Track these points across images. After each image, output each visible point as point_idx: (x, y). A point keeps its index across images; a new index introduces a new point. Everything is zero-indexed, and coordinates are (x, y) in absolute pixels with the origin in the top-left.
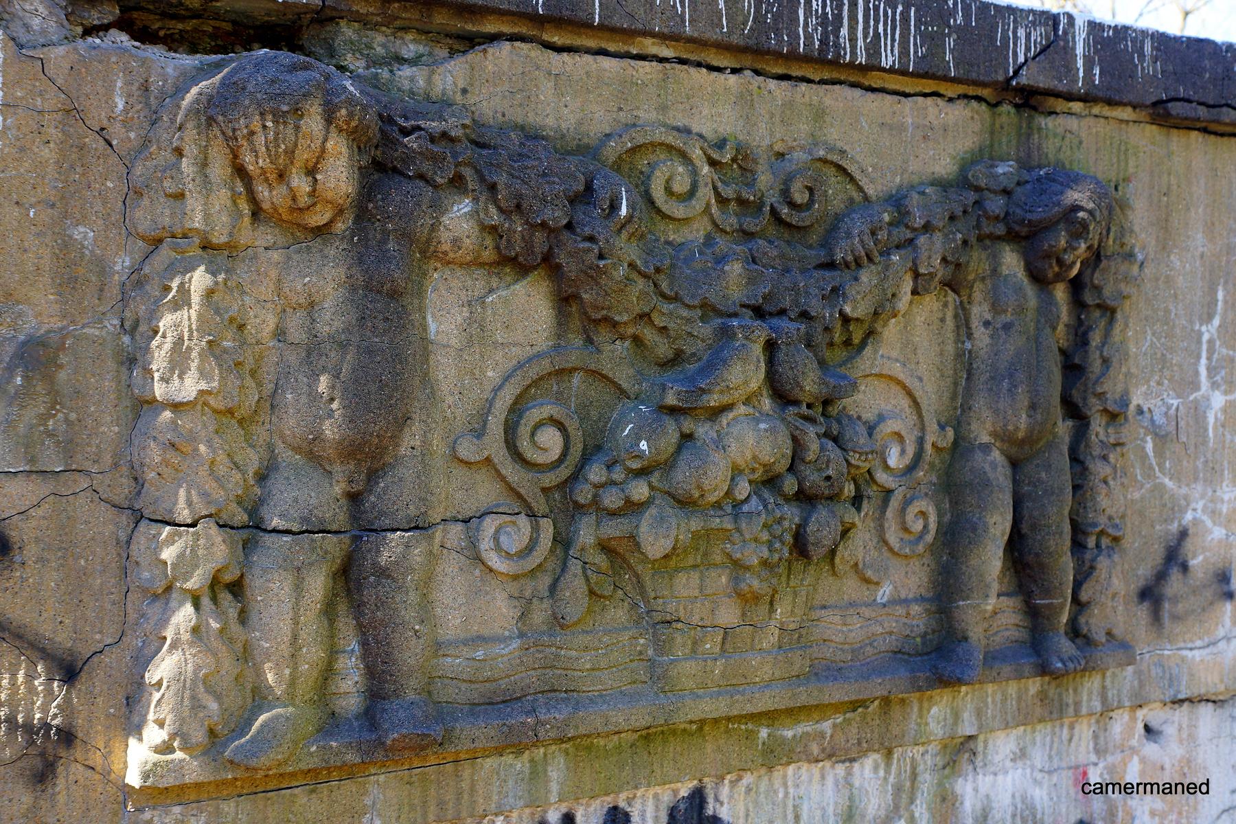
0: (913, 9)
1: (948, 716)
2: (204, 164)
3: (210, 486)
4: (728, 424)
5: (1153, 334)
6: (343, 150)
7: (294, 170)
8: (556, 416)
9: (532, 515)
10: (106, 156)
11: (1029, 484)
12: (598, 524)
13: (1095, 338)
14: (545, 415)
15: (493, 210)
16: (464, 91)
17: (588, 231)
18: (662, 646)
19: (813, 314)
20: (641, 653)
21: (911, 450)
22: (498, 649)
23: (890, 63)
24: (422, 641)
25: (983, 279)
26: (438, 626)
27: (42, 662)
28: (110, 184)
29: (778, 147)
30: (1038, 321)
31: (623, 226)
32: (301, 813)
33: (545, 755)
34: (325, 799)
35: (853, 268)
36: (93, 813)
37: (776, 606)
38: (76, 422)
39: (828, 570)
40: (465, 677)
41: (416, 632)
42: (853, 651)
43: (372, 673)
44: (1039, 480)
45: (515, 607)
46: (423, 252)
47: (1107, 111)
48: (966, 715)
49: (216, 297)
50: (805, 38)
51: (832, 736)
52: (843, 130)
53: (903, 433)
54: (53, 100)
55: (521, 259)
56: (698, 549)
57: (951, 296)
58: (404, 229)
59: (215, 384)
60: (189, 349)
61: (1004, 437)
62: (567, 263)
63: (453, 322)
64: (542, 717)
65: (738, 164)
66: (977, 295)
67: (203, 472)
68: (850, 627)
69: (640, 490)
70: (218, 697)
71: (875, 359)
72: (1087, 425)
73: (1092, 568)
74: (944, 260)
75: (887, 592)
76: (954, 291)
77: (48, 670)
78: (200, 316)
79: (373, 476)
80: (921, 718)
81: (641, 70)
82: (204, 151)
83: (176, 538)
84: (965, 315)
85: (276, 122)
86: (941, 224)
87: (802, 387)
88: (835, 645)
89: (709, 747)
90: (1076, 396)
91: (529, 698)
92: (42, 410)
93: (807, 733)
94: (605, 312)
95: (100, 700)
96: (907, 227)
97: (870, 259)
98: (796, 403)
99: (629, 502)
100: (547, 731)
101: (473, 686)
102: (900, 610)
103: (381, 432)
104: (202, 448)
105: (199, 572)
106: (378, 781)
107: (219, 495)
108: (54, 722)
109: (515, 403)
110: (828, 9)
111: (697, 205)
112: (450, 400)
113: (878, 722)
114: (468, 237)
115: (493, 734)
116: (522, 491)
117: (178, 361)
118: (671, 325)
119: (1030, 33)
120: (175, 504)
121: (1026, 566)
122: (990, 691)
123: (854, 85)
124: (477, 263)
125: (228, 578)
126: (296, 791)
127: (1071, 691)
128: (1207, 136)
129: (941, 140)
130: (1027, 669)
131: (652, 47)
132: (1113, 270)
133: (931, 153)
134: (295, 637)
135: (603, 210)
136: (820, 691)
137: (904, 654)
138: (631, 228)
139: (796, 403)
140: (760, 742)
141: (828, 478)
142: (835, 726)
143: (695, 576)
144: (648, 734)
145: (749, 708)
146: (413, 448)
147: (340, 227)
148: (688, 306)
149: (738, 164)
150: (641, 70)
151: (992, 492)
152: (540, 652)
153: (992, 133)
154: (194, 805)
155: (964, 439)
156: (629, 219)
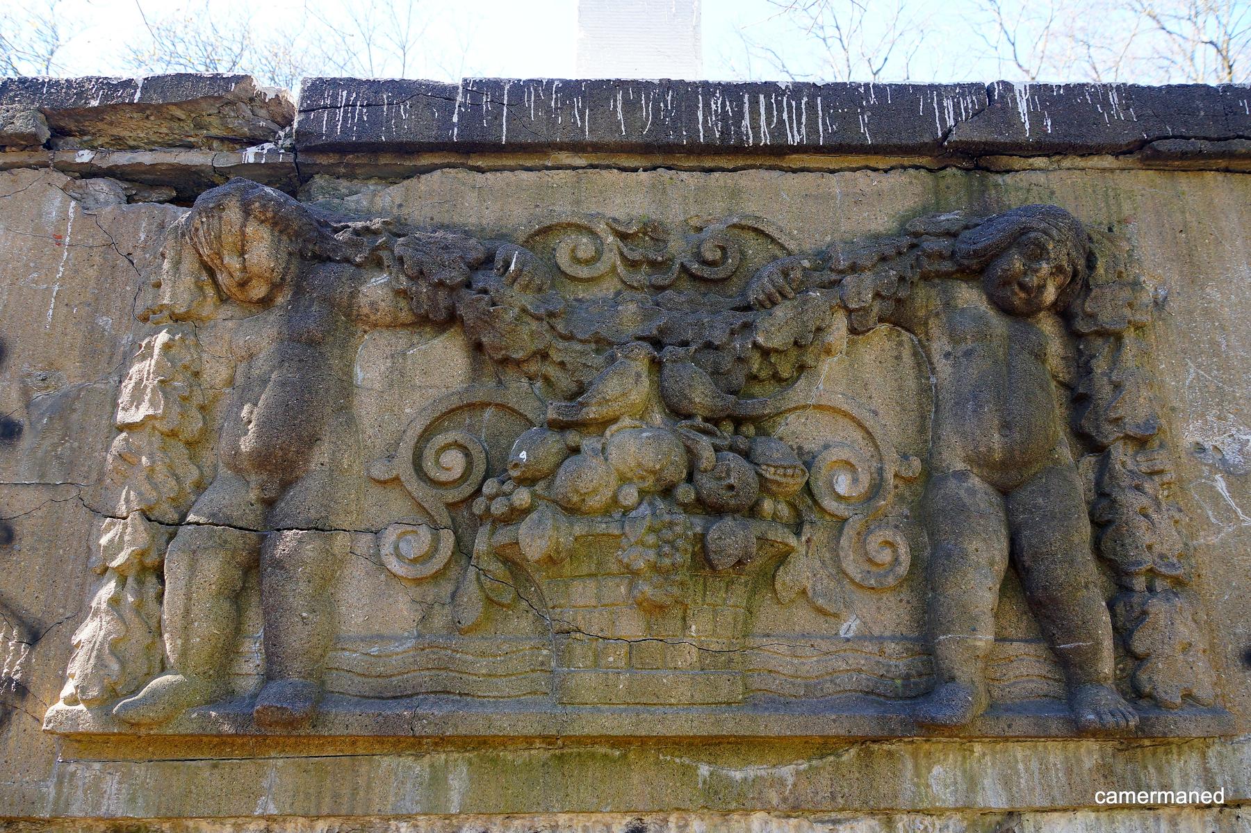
0: (819, 98)
1: (959, 780)
2: (177, 264)
3: (146, 487)
4: (612, 435)
5: (1199, 367)
6: (265, 235)
7: (225, 252)
8: (461, 441)
9: (435, 528)
10: (128, 271)
11: (1023, 513)
12: (493, 533)
13: (1100, 366)
14: (450, 440)
15: (403, 278)
16: (400, 206)
17: (481, 285)
18: (564, 656)
19: (716, 343)
20: (542, 664)
21: (865, 481)
22: (393, 647)
23: (797, 139)
24: (309, 628)
25: (937, 314)
26: (342, 623)
27: (17, 627)
28: (128, 288)
29: (695, 222)
30: (1010, 348)
31: (514, 280)
32: (202, 786)
33: (446, 761)
34: (226, 776)
35: (769, 306)
36: (32, 760)
37: (689, 623)
38: (77, 449)
39: (772, 598)
40: (359, 670)
41: (303, 618)
42: (806, 686)
43: (270, 657)
44: (1035, 506)
45: (416, 610)
46: (348, 315)
47: (1080, 162)
48: (987, 782)
49: (173, 351)
50: (705, 131)
51: (795, 785)
52: (762, 203)
53: (852, 461)
54: (101, 238)
55: (431, 316)
56: (591, 557)
57: (906, 336)
58: (325, 295)
59: (160, 411)
60: (146, 386)
61: (980, 461)
62: (466, 313)
63: (377, 370)
64: (419, 711)
65: (649, 236)
66: (935, 330)
67: (141, 477)
68: (803, 660)
69: (522, 497)
70: (123, 663)
71: (810, 391)
72: (1108, 455)
73: (1145, 613)
74: (877, 295)
75: (853, 627)
76: (908, 330)
77: (20, 634)
78: (157, 363)
79: (286, 486)
80: (918, 777)
81: (556, 177)
82: (179, 253)
83: (112, 527)
84: (925, 352)
85: (207, 217)
86: (869, 264)
87: (690, 399)
88: (783, 678)
89: (636, 778)
90: (1088, 427)
91: (420, 697)
92: (56, 440)
93: (762, 777)
94: (504, 352)
95: (52, 663)
96: (832, 270)
97: (784, 297)
98: (689, 416)
99: (513, 509)
100: (424, 727)
101: (366, 680)
102: (869, 647)
103: (284, 446)
104: (144, 459)
105: (123, 553)
106: (276, 765)
107: (152, 496)
108: (16, 677)
109: (425, 430)
110: (728, 108)
111: (601, 267)
112: (370, 432)
113: (857, 775)
114: (383, 301)
115: (367, 722)
116: (426, 505)
117: (136, 399)
118: (567, 359)
119: (959, 102)
120: (119, 502)
121: (1040, 604)
122: (1019, 756)
123: (771, 168)
124: (394, 325)
125: (151, 560)
126: (200, 763)
127: (1152, 770)
128: (1229, 175)
129: (876, 203)
130: (1054, 727)
131: (565, 158)
132: (1109, 296)
133: (866, 215)
134: (187, 611)
135: (499, 270)
136: (752, 720)
137: (879, 695)
138: (523, 280)
139: (689, 416)
140: (700, 780)
141: (731, 487)
142: (798, 773)
143: (591, 585)
144: (562, 754)
145: (660, 730)
146: (322, 464)
147: (280, 300)
148: (581, 341)
149: (649, 236)
150: (556, 177)
151: (969, 517)
152: (434, 653)
153: (936, 193)
154: (111, 764)
155: (937, 469)
156: (519, 272)
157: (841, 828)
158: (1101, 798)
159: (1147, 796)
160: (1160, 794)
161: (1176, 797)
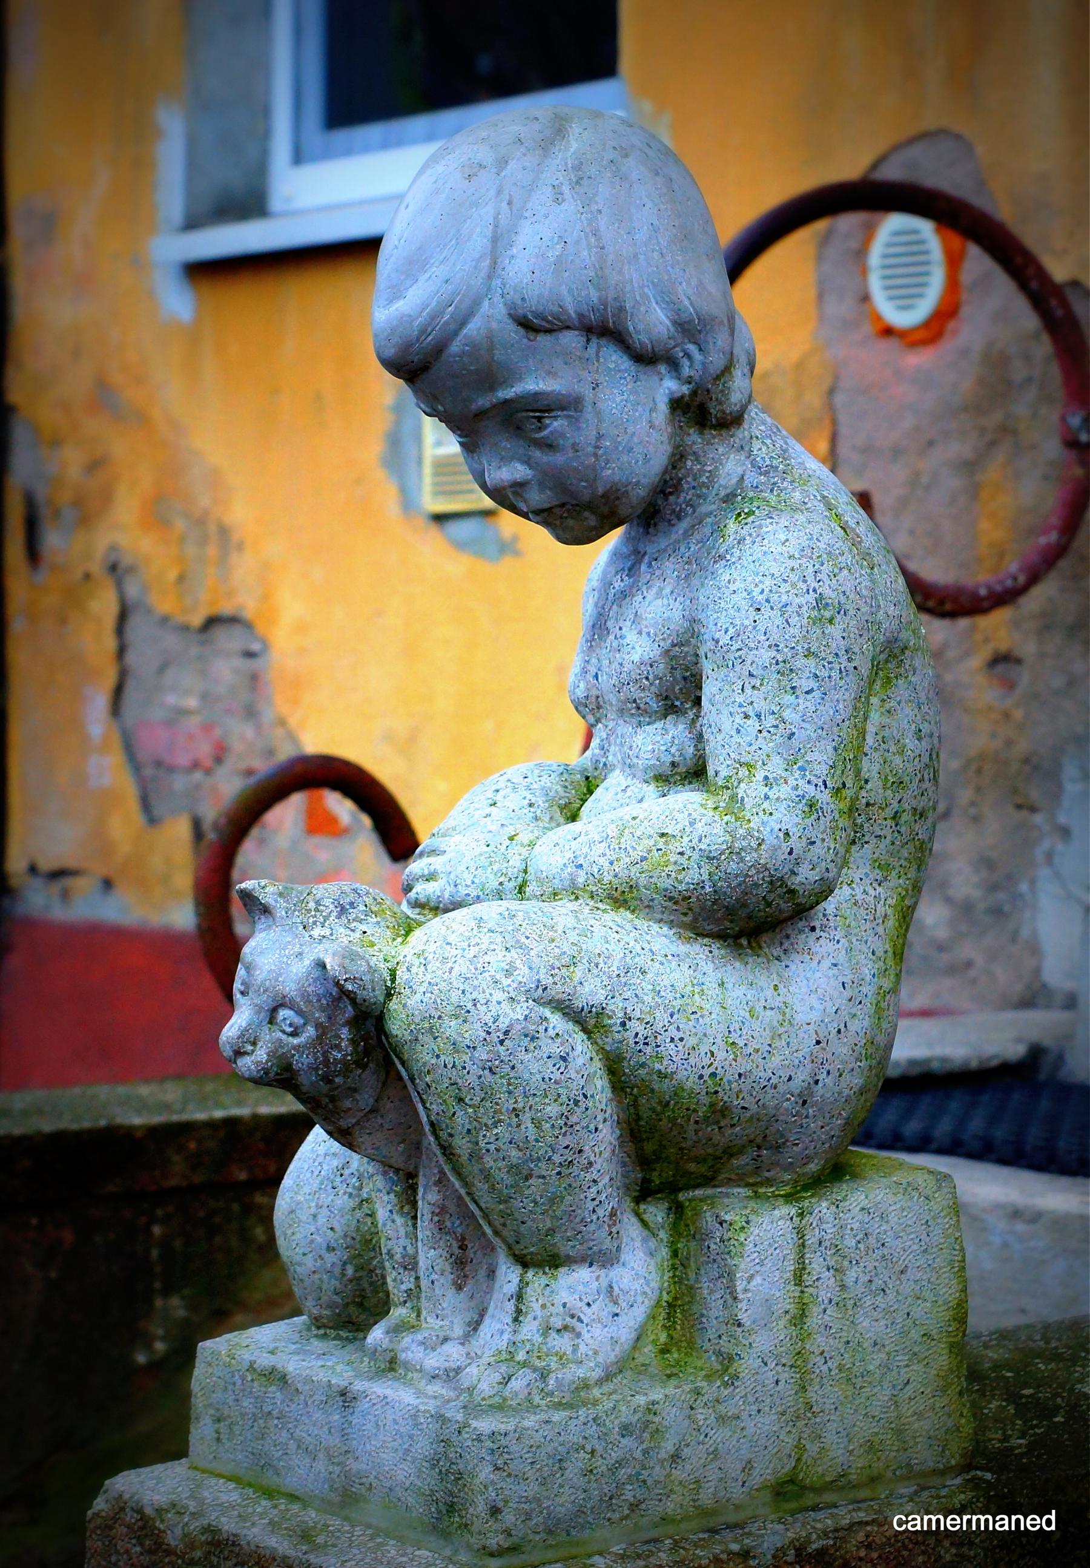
157: (931, 1464)
158: (900, 1525)
159: (959, 1521)
160: (975, 1518)
161: (995, 1522)
